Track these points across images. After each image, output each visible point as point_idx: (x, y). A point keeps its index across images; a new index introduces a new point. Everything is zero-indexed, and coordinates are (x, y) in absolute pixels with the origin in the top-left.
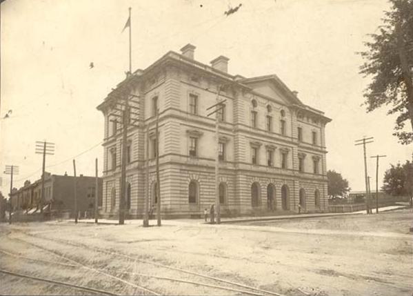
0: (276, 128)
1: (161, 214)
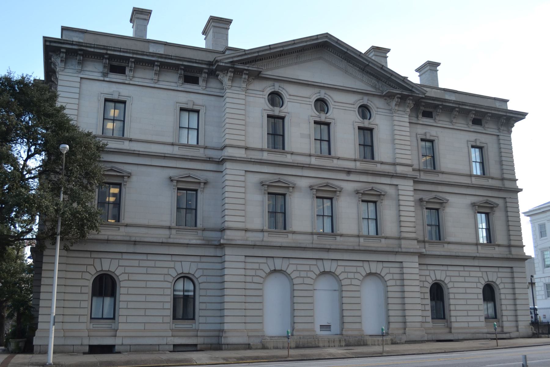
0: (346, 142)
1: (540, 332)
